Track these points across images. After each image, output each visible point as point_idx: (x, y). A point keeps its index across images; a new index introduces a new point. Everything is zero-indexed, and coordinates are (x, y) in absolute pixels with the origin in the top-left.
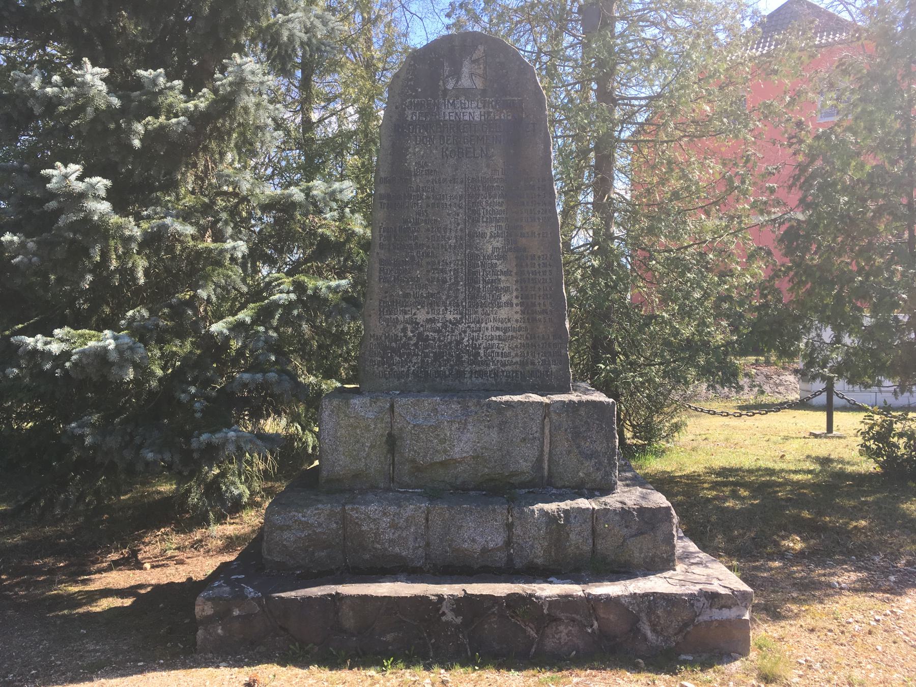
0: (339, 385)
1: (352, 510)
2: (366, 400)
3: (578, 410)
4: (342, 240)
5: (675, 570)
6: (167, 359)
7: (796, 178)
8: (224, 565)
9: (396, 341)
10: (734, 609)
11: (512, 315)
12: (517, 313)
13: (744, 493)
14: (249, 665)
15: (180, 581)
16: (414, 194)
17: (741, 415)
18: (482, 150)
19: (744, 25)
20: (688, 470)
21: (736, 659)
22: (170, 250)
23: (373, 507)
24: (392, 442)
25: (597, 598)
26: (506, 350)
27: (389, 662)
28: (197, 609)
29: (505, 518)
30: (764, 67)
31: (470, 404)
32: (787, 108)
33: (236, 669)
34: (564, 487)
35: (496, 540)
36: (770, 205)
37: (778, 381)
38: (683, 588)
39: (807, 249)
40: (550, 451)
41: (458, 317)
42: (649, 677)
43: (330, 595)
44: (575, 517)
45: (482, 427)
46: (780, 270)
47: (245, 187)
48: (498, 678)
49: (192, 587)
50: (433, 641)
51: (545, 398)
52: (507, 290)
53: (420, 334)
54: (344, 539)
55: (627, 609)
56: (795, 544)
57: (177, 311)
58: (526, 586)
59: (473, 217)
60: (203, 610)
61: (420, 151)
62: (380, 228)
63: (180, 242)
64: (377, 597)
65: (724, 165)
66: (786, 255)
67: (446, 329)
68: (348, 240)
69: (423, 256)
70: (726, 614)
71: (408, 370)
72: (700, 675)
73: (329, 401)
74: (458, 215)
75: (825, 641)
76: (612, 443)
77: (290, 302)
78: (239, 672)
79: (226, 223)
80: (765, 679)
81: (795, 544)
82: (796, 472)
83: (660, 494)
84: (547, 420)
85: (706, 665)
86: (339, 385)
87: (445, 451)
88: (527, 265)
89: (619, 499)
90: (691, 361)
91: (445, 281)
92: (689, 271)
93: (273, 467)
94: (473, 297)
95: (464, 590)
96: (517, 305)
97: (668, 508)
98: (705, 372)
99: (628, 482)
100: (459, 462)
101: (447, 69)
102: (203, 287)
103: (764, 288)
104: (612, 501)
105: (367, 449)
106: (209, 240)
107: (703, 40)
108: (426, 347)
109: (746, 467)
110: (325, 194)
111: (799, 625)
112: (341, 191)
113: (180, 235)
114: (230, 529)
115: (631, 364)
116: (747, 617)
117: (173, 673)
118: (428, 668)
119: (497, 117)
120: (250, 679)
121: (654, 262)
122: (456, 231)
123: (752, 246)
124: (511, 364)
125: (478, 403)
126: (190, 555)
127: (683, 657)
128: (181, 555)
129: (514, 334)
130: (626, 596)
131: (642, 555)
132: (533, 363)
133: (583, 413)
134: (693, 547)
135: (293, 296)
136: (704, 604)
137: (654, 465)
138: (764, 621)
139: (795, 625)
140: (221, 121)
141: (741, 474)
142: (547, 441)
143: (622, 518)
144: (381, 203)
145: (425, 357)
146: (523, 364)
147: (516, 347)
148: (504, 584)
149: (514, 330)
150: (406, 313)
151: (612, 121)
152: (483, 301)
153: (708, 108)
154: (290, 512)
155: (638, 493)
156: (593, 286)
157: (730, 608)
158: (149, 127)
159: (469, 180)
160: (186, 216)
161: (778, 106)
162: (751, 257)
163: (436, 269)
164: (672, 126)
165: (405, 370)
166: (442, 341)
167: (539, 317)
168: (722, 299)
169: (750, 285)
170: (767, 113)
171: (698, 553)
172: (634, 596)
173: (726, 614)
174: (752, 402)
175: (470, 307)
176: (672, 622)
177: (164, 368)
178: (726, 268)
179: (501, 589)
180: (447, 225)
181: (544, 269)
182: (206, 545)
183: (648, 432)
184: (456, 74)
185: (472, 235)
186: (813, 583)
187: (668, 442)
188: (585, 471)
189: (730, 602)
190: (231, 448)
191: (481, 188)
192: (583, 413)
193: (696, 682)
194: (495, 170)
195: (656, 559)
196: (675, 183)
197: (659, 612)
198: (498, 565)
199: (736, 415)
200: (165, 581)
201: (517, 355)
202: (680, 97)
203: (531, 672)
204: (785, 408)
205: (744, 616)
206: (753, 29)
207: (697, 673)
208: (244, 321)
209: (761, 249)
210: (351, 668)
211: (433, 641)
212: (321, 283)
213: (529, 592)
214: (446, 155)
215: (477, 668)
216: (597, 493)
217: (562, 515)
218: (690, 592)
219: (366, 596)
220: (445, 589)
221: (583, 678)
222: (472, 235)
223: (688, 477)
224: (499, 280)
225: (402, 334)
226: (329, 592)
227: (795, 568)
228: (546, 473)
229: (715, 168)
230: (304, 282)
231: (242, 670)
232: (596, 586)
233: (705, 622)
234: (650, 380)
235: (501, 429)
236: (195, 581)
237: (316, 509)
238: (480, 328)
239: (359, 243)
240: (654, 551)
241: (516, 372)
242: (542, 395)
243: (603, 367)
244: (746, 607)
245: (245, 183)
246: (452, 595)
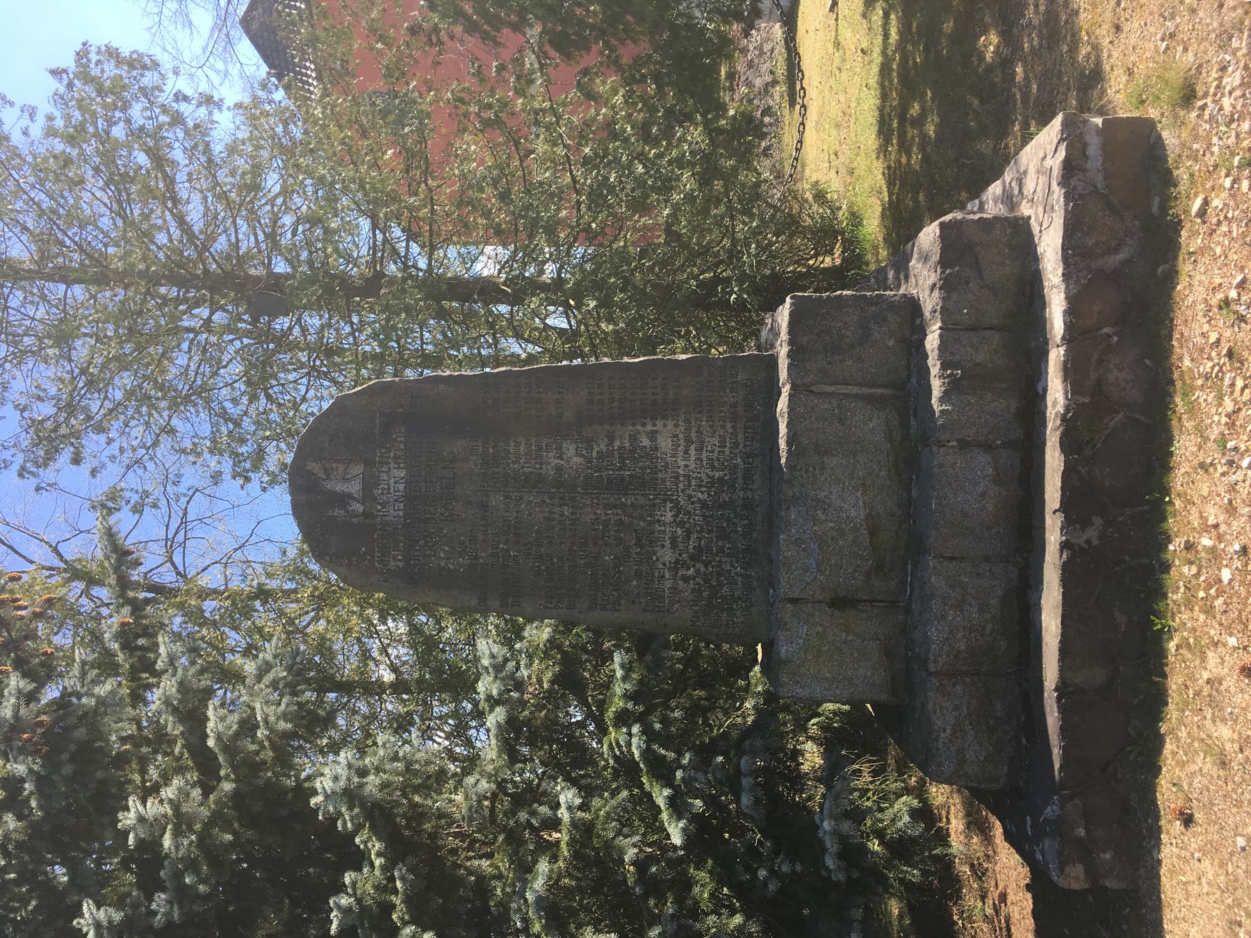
0: (757, 668)
1: (935, 662)
2: (782, 636)
4: (559, 656)
5: (1029, 217)
6: (719, 905)
7: (485, 37)
8: (1008, 837)
9: (700, 591)
10: (1088, 138)
12: (665, 425)
13: (915, 109)
14: (1157, 817)
15: (1031, 901)
16: (501, 560)
17: (804, 106)
18: (444, 468)
19: (280, 102)
20: (881, 182)
21: (1160, 137)
22: (569, 892)
23: (933, 633)
24: (840, 603)
25: (1068, 327)
26: (716, 441)
27: (1157, 621)
28: (1076, 886)
29: (951, 451)
30: (334, 76)
31: (790, 494)
32: (392, 46)
33: (1162, 836)
34: (908, 367)
35: (983, 463)
36: (521, 70)
37: (757, 53)
38: (1056, 208)
39: (581, 23)
40: (857, 385)
41: (669, 505)
42: (1184, 260)
43: (1059, 699)
44: (951, 353)
45: (823, 478)
46: (609, 57)
47: (484, 785)
48: (1183, 470)
49: (1039, 885)
50: (1127, 558)
51: (784, 390)
52: (634, 438)
53: (692, 558)
54: (978, 674)
56: (990, 44)
57: (654, 887)
58: (1050, 426)
60: (1077, 878)
62: (547, 607)
63: (558, 880)
64: (1062, 635)
65: (465, 130)
66: (588, 49)
67: (685, 523)
68: (559, 648)
69: (585, 551)
70: (1094, 146)
71: (741, 575)
72: (1182, 188)
73: (782, 686)
74: (531, 502)
75: (1133, 11)
76: (847, 300)
77: (643, 732)
78: (1168, 833)
79: (533, 813)
80: (1188, 99)
81: (990, 43)
82: (886, 36)
83: (921, 235)
85: (1168, 180)
86: (757, 668)
87: (855, 530)
89: (927, 293)
90: (729, 178)
91: (620, 522)
92: (606, 178)
93: (869, 761)
95: (1054, 513)
96: (654, 425)
97: (942, 225)
98: (745, 157)
99: (902, 277)
100: (871, 510)
101: (339, 512)
102: (622, 852)
103: (631, 79)
104: (930, 302)
105: (850, 638)
106: (556, 835)
107: (302, 160)
108: (709, 549)
109: (878, 102)
110: (496, 677)
111: (1110, 46)
112: (493, 656)
113: (550, 878)
114: (956, 825)
115: (730, 257)
116: (1098, 121)
117: (1167, 926)
118: (1166, 567)
119: (402, 446)
120: (1178, 819)
121: (594, 225)
122: (553, 505)
123: (574, 94)
124: (734, 435)
126: (993, 883)
127: (1155, 210)
128: (994, 895)
129: (694, 429)
130: (1067, 288)
132: (735, 405)
133: (805, 339)
134: (995, 188)
135: (636, 729)
136: (1080, 180)
137: (872, 227)
138: (1103, 93)
139: (1109, 50)
140: (398, 819)
141: (887, 110)
142: (843, 389)
144: (513, 605)
145: (724, 552)
146: (735, 419)
147: (711, 427)
148: (1047, 456)
149: (688, 429)
150: (663, 576)
151: (404, 280)
153: (390, 152)
154: (938, 749)
155: (920, 266)
156: (624, 309)
157: (1085, 145)
158: (406, 917)
159: (484, 486)
160: (525, 869)
161: (390, 56)
162: (590, 96)
164: (412, 200)
165: (740, 579)
166: (702, 527)
168: (646, 137)
169: (628, 96)
170: (397, 72)
171: (1004, 182)
173: (1094, 146)
174: (784, 88)
175: (655, 489)
177: (733, 913)
178: (603, 129)
179: (1054, 461)
180: (544, 517)
182: (978, 858)
183: (826, 235)
186: (1047, 22)
187: (840, 208)
190: (846, 826)
191: (496, 470)
193: (1192, 195)
196: (489, 196)
199: (803, 112)
200: (1030, 923)
201: (723, 427)
202: (376, 191)
203: (1174, 423)
204: (795, 45)
205: (1097, 125)
206: (287, 88)
207: (1179, 193)
208: (668, 797)
209: (579, 83)
210: (1164, 676)
211: (1127, 558)
212: (618, 689)
213: (1059, 422)
214: (450, 515)
215: (1167, 499)
216: (918, 321)
217: (949, 372)
218: (1062, 200)
219: (1060, 650)
220: (1052, 538)
221: (1185, 351)
223: (890, 183)
224: (620, 448)
225: (692, 582)
226: (1054, 701)
227: (1026, 45)
228: (888, 391)
229: (471, 144)
230: (616, 712)
231: (1164, 829)
232: (1052, 327)
234: (755, 233)
236: (1031, 879)
237: (935, 713)
239: (563, 633)
241: (745, 427)
242: (779, 394)
243: (734, 296)
244: (1085, 122)
245: (479, 786)
246: (1062, 530)
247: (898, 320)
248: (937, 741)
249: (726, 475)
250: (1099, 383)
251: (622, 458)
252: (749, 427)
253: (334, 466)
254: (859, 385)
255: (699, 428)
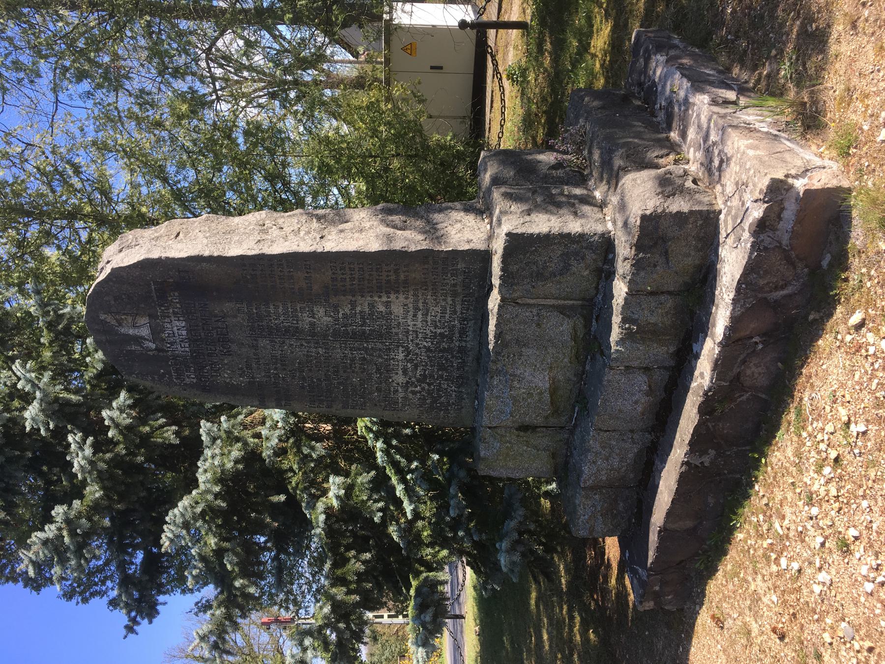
1: (585, 482)
3: (512, 273)
5: (720, 212)
10: (786, 204)
11: (400, 302)
16: (273, 380)
23: (586, 469)
26: (438, 309)
34: (597, 288)
41: (401, 349)
52: (372, 306)
53: (418, 380)
55: (748, 309)
59: (294, 332)
61: (227, 373)
70: (789, 214)
71: (455, 391)
74: (292, 345)
84: (519, 301)
87: (541, 393)
88: (344, 286)
91: (364, 359)
94: (381, 336)
108: (432, 376)
124: (454, 305)
125: (494, 362)
127: (825, 263)
130: (733, 309)
131: (693, 253)
132: (455, 285)
133: (516, 267)
136: (769, 236)
143: (644, 269)
146: (455, 295)
149: (416, 301)
150: (397, 391)
152: (384, 327)
154: (578, 523)
157: (783, 209)
163: (351, 365)
165: (454, 393)
167: (402, 277)
172: (735, 301)
173: (789, 214)
175: (390, 339)
176: (778, 270)
181: (347, 269)
184: (138, 340)
185: (313, 334)
188: (582, 271)
189: (776, 209)
192: (516, 267)
194: (238, 310)
195: (702, 235)
197: (762, 282)
198: (667, 377)
216: (611, 256)
217: (627, 326)
222: (313, 334)
224: (361, 312)
225: (418, 394)
232: (714, 326)
233: (790, 239)
235: (524, 345)
238: (413, 331)
240: (690, 238)
246: (686, 454)
247: (594, 257)
248: (578, 519)
249: (446, 331)
250: (738, 377)
251: (363, 318)
252: (465, 301)
253: (123, 317)
254: (556, 298)
255: (425, 300)
